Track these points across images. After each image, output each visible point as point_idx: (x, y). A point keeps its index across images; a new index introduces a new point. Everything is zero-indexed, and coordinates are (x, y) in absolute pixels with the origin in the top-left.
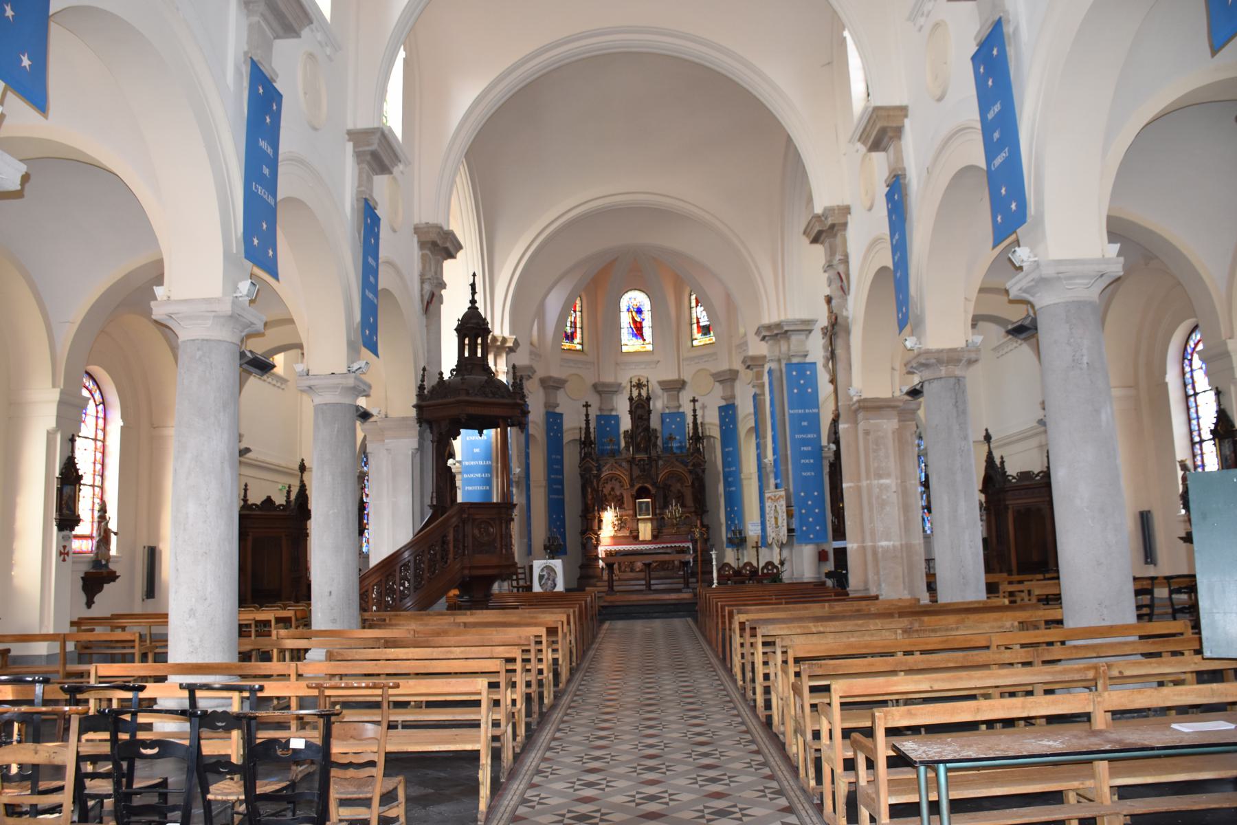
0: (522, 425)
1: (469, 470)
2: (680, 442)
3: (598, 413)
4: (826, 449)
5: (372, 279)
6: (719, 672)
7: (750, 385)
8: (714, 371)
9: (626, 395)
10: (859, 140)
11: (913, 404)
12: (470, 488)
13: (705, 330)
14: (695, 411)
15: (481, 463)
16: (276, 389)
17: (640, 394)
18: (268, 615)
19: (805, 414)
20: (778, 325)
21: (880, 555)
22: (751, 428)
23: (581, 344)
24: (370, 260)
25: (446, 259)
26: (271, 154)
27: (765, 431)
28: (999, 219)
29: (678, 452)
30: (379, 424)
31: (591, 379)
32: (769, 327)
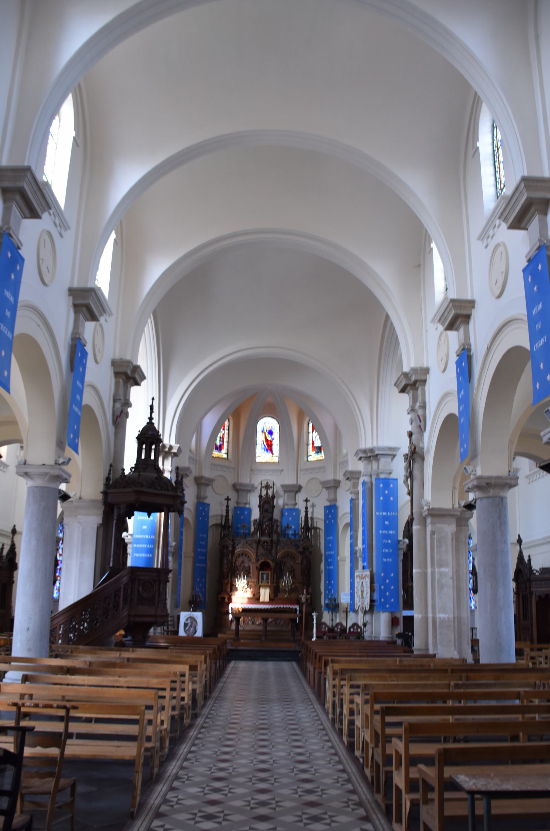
0: (180, 512)
1: (137, 541)
5: (78, 397)
7: (349, 492)
9: (257, 493)
12: (137, 555)
13: (318, 450)
14: (307, 508)
15: (147, 537)
17: (267, 493)
20: (372, 450)
21: (438, 624)
25: (133, 386)
28: (538, 386)
29: (293, 538)
30: (74, 503)
31: (231, 480)
32: (365, 451)
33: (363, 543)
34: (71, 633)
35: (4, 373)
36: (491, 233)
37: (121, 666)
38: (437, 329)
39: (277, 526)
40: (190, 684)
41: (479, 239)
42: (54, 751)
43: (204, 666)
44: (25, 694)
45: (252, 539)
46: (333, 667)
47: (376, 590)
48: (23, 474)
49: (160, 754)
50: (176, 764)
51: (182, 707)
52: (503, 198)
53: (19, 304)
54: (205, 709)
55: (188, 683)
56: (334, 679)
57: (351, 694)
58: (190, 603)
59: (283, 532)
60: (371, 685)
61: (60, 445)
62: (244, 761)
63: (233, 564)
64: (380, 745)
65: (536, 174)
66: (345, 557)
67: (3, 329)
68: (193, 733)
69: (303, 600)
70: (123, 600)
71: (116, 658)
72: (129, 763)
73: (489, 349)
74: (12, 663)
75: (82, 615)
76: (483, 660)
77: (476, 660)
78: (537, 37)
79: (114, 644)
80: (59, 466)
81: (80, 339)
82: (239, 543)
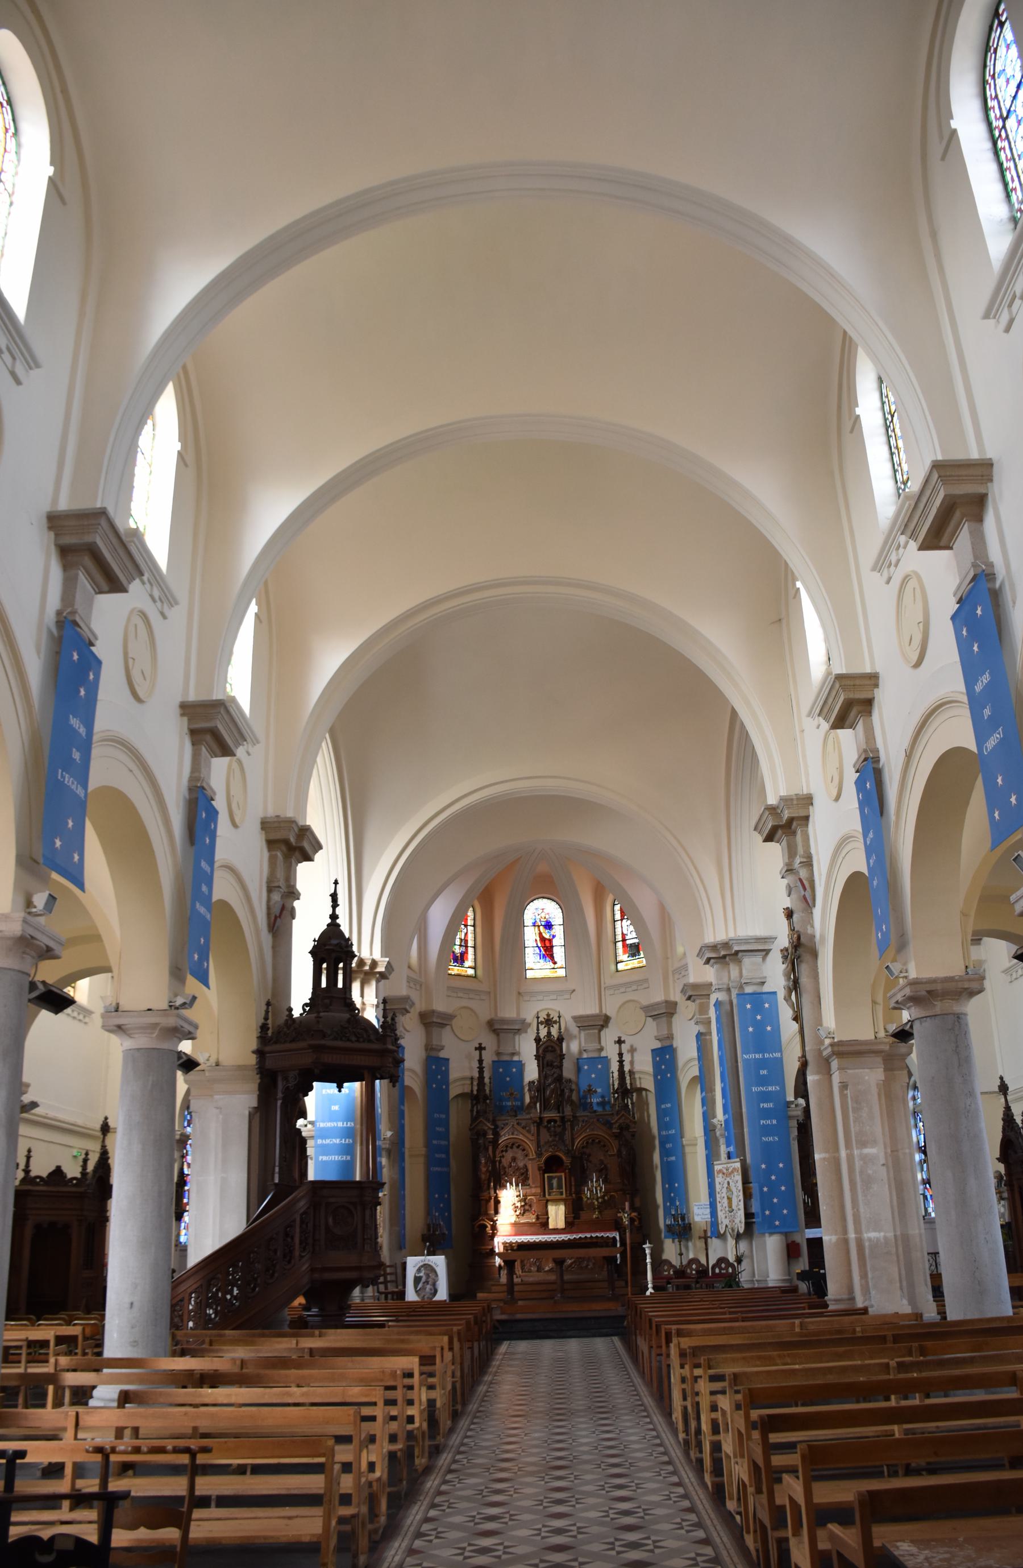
0: (394, 1078)
1: (324, 1133)
2: (603, 1097)
3: (496, 1059)
4: (793, 1106)
5: (204, 888)
6: (655, 1419)
7: (693, 1022)
8: (645, 1003)
9: (531, 1034)
10: (819, 715)
11: (902, 1047)
12: (325, 1158)
13: (634, 950)
14: (621, 1055)
15: (340, 1124)
16: (76, 1022)
17: (549, 1033)
18: (46, 1332)
19: (764, 1059)
20: (726, 945)
21: (867, 1251)
22: (695, 1078)
23: (474, 968)
24: (203, 864)
25: (301, 862)
26: (84, 734)
27: (713, 1083)
28: (996, 815)
29: (600, 1109)
30: (207, 1074)
31: (485, 1014)
32: (714, 947)
33: (725, 1111)
34: (211, 1308)
35: (73, 858)
36: (893, 558)
37: (298, 1364)
38: (818, 727)
39: (571, 1091)
40: (424, 1389)
41: (874, 569)
42: (171, 1534)
43: (448, 1356)
44: (126, 1428)
45: (528, 1117)
46: (679, 1343)
47: (754, 1196)
48: (115, 1028)
49: (370, 1527)
50: (400, 1545)
51: (410, 1435)
52: (908, 497)
53: (95, 738)
54: (455, 1436)
55: (420, 1389)
56: (682, 1367)
57: (713, 1393)
58: (425, 1238)
59: (583, 1101)
60: (745, 1374)
61: (177, 974)
62: (524, 1533)
63: (498, 1163)
64: (764, 1489)
65: (958, 455)
66: (696, 1139)
67: (68, 782)
68: (431, 1483)
69: (626, 1221)
70: (301, 1243)
71: (290, 1350)
72: (311, 1548)
73: (909, 756)
74: (105, 1371)
75: (228, 1274)
76: (952, 1315)
77: (942, 1313)
78: (934, 235)
79: (288, 1323)
80: (176, 1011)
81: (203, 788)
82: (506, 1124)
